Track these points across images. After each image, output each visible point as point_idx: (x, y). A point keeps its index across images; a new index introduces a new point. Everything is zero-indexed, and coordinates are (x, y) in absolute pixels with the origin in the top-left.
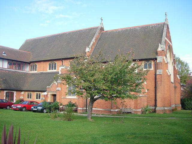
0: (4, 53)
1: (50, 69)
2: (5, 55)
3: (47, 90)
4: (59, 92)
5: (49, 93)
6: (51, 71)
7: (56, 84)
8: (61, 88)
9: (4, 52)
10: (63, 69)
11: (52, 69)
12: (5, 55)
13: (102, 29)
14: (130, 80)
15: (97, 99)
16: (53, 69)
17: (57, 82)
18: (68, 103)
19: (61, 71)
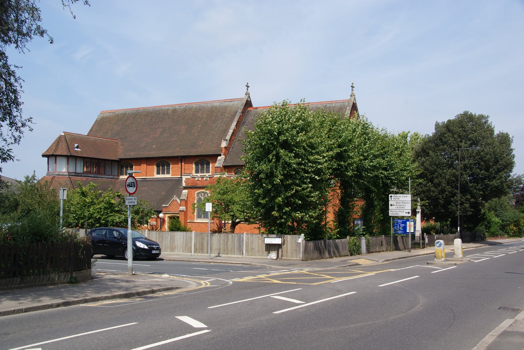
0: (77, 147)
1: (158, 173)
2: (79, 150)
3: (164, 209)
4: (183, 213)
5: (167, 215)
6: (161, 176)
7: (179, 201)
8: (187, 208)
9: (76, 145)
10: (188, 179)
11: (163, 173)
12: (79, 150)
13: (248, 104)
14: (324, 121)
15: (239, 222)
16: (164, 174)
17: (179, 198)
18: (23, 180)
19: (185, 182)
